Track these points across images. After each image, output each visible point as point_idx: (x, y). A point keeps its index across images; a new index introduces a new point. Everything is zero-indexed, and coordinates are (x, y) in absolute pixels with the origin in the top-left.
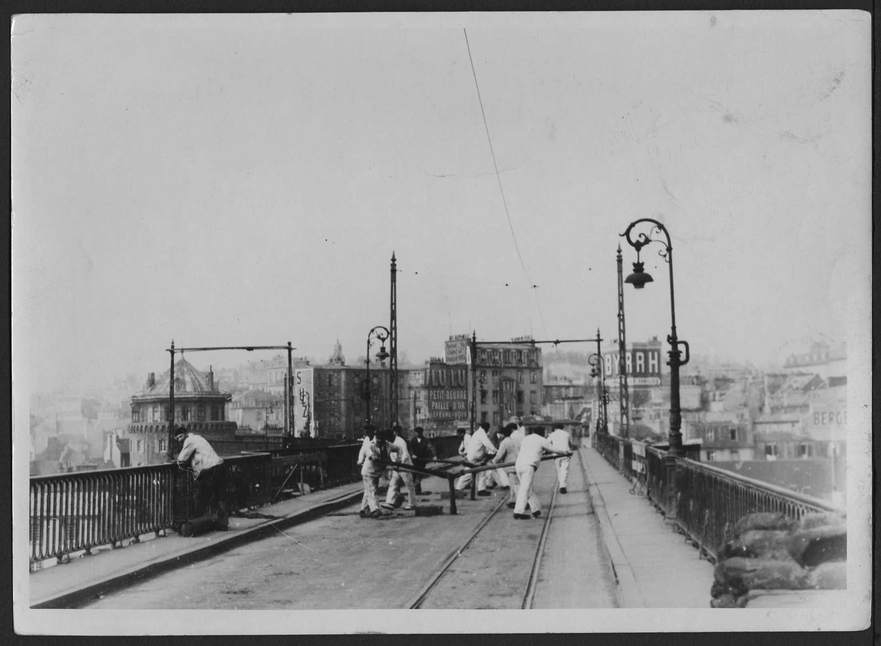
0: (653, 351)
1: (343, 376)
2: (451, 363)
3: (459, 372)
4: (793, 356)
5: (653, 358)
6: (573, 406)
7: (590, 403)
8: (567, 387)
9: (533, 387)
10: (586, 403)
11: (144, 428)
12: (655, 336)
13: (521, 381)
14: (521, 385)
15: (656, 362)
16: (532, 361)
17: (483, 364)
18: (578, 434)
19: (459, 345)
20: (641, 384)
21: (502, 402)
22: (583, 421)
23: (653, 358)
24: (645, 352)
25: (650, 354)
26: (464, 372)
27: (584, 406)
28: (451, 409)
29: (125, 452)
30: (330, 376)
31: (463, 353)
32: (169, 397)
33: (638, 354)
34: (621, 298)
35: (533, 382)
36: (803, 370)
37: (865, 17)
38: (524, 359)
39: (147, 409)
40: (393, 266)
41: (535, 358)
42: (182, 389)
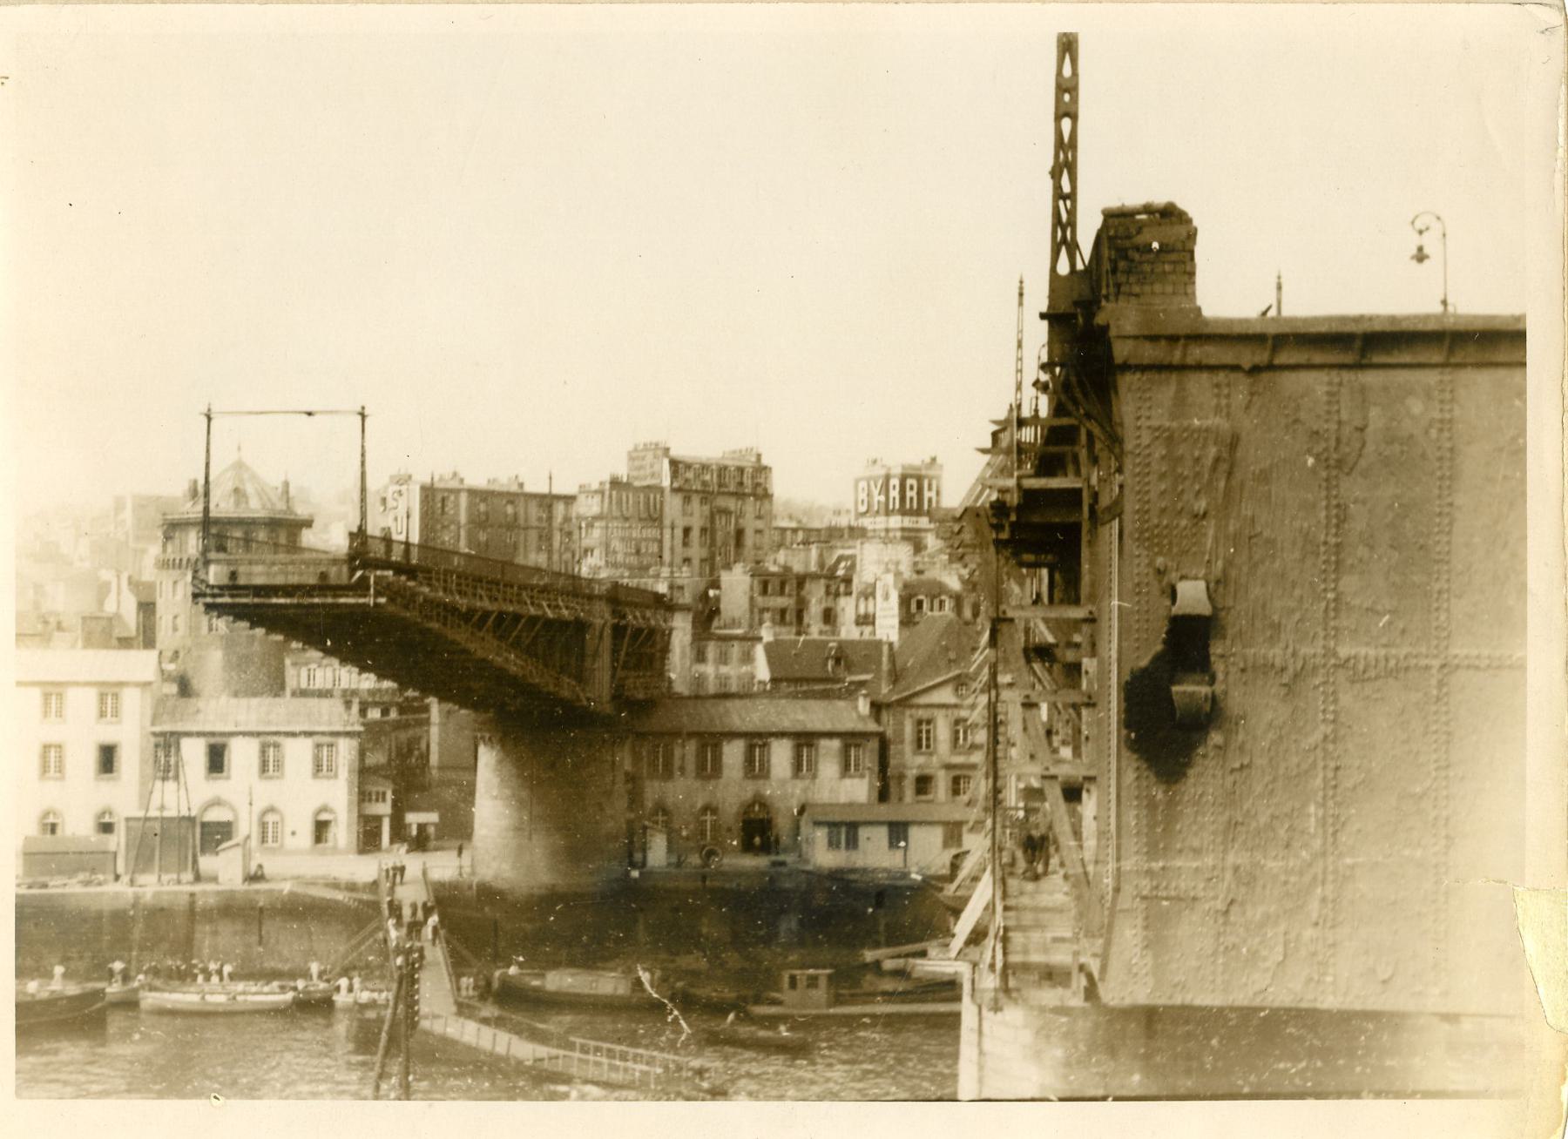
1: (464, 499)
3: (652, 496)
5: (911, 499)
7: (854, 547)
8: (795, 531)
9: (760, 524)
10: (843, 548)
11: (184, 562)
12: (1414, 262)
13: (741, 515)
14: (741, 521)
15: (933, 494)
16: (758, 485)
17: (687, 487)
18: (414, 832)
19: (650, 456)
20: (911, 525)
21: (713, 543)
22: (840, 572)
26: (658, 496)
27: (840, 552)
28: (638, 552)
29: (143, 600)
30: (443, 500)
31: (656, 468)
32: (201, 515)
33: (909, 482)
35: (759, 517)
38: (747, 481)
39: (187, 535)
40: (1021, 288)
41: (762, 480)
42: (243, 505)
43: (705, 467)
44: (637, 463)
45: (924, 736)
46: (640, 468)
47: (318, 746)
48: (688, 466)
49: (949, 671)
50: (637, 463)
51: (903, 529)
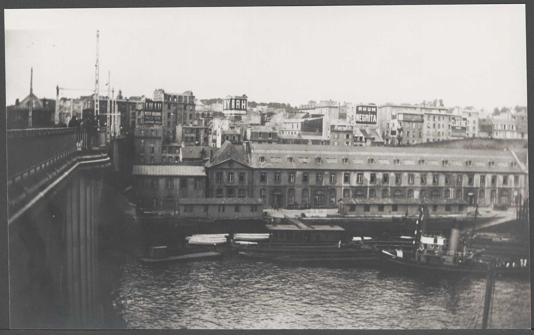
0: (244, 100)
2: (156, 100)
4: (302, 105)
5: (244, 103)
6: (207, 121)
15: (244, 104)
23: (244, 103)
24: (241, 100)
25: (242, 101)
33: (237, 101)
34: (97, 70)
36: (303, 111)
37: (521, 9)
43: (175, 97)
44: (156, 95)
45: (359, 178)
46: (157, 96)
47: (358, 174)
48: (170, 96)
49: (228, 158)
50: (156, 95)
51: (235, 114)
